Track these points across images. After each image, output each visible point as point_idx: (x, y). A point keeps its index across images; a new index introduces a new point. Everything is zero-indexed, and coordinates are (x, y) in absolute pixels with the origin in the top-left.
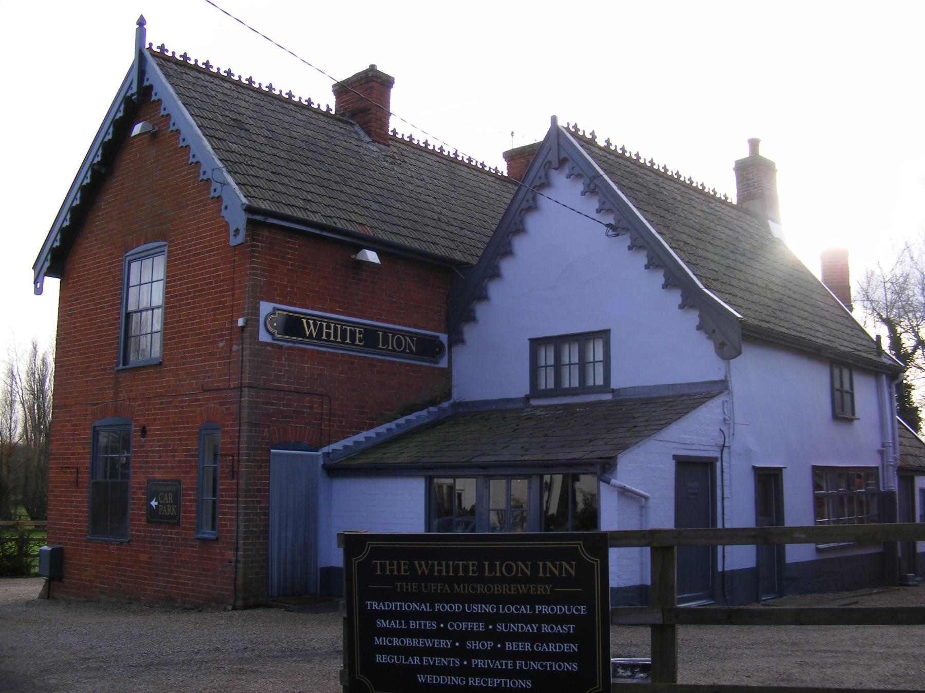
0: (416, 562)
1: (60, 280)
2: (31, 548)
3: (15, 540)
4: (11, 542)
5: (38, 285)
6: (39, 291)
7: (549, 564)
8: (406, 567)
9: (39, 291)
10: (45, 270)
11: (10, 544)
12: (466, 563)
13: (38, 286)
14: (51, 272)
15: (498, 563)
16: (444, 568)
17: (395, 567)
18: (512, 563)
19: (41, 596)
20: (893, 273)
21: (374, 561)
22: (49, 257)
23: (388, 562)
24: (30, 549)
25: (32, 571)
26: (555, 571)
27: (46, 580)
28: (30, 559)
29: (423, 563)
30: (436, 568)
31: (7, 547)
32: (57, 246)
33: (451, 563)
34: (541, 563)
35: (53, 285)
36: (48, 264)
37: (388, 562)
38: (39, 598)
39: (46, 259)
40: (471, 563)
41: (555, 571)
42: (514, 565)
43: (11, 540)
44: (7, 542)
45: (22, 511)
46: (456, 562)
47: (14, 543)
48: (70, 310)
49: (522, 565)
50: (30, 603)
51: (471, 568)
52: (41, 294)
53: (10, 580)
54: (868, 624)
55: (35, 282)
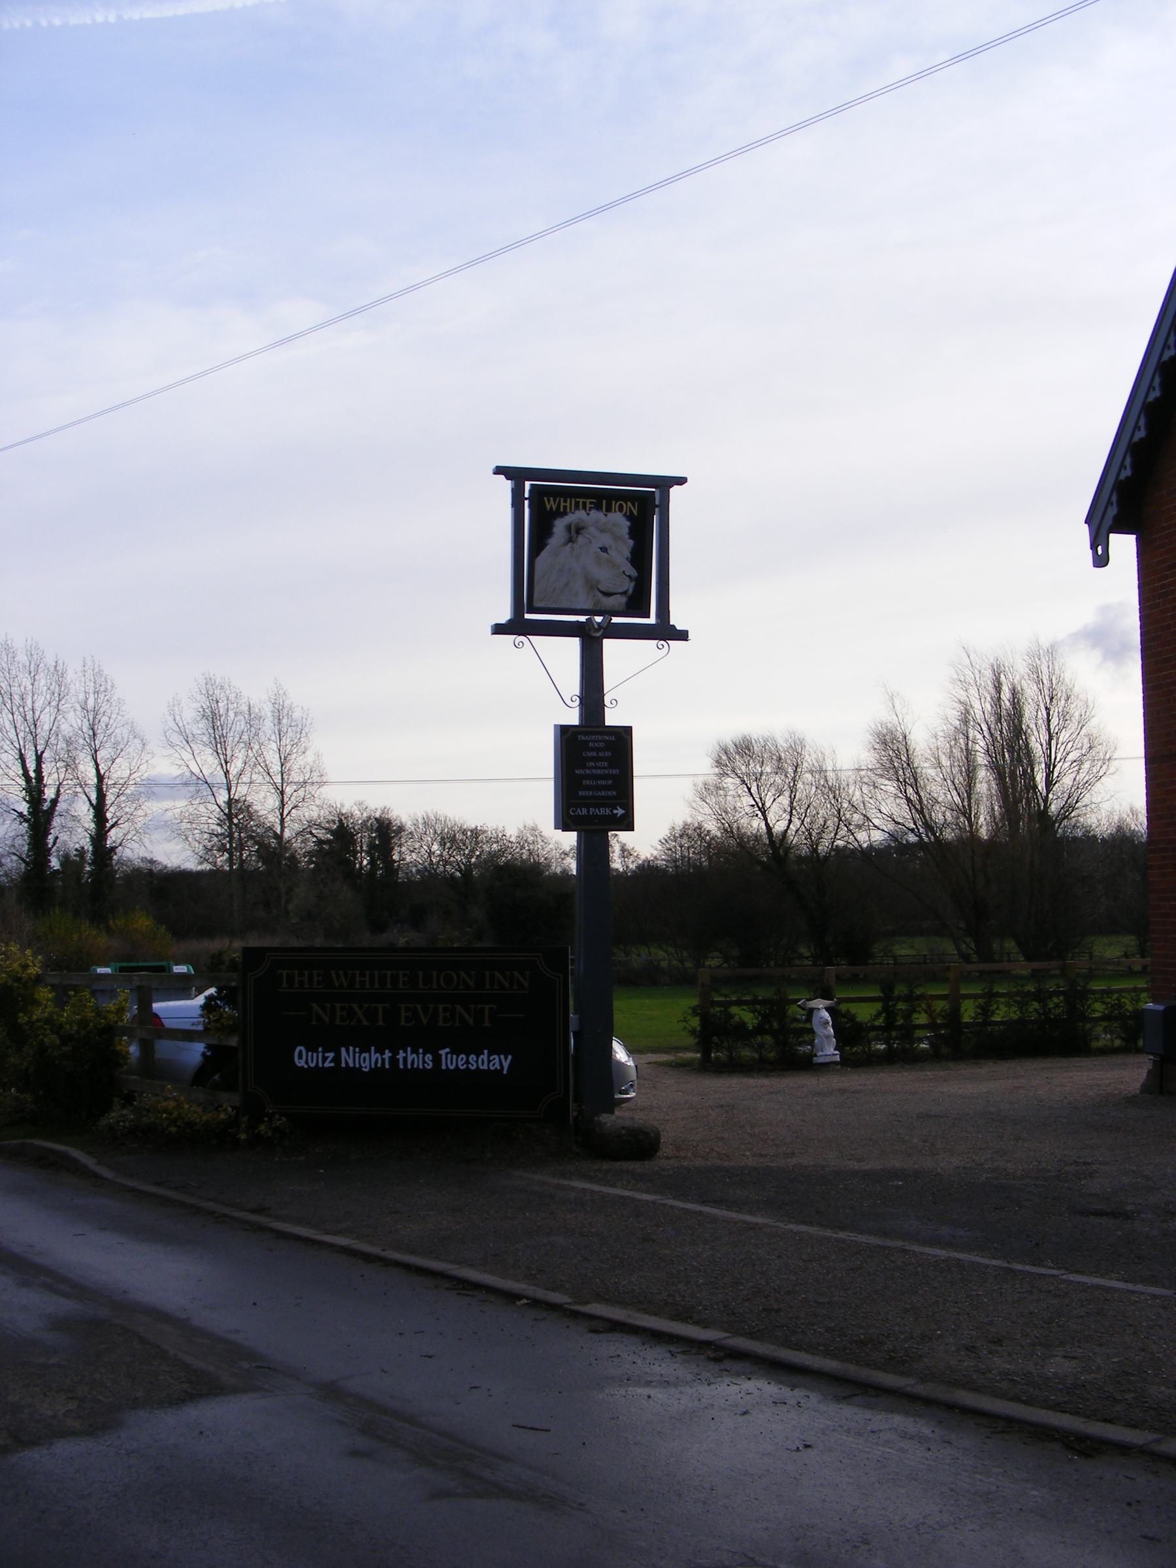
0: (333, 972)
1: (1133, 538)
2: (1090, 1006)
3: (1062, 993)
4: (1058, 997)
5: (1100, 549)
6: (1101, 561)
7: (497, 974)
8: (320, 978)
9: (1101, 561)
10: (1108, 521)
11: (1055, 1000)
12: (289, 971)
13: (1100, 552)
14: (1121, 527)
15: (435, 973)
16: (367, 979)
17: (306, 978)
18: (452, 973)
19: (1146, 1089)
20: (20, 776)
21: (279, 971)
22: (1114, 498)
23: (296, 972)
24: (1088, 1008)
25: (1094, 1044)
26: (504, 982)
27: (1155, 1061)
28: (1088, 1026)
29: (341, 972)
30: (358, 979)
31: (1052, 1006)
32: (1127, 478)
33: (376, 973)
34: (488, 973)
35: (1124, 546)
36: (1113, 511)
37: (296, 972)
38: (1141, 1093)
39: (1109, 503)
40: (401, 973)
41: (504, 982)
42: (455, 976)
43: (1057, 993)
44: (1050, 997)
45: (1010, 944)
46: (383, 972)
47: (1062, 998)
48: (1163, 586)
49: (500, 977)
50: (1131, 1100)
51: (401, 979)
52: (1107, 564)
53: (1064, 1062)
54: (613, 1020)
55: (1094, 547)
